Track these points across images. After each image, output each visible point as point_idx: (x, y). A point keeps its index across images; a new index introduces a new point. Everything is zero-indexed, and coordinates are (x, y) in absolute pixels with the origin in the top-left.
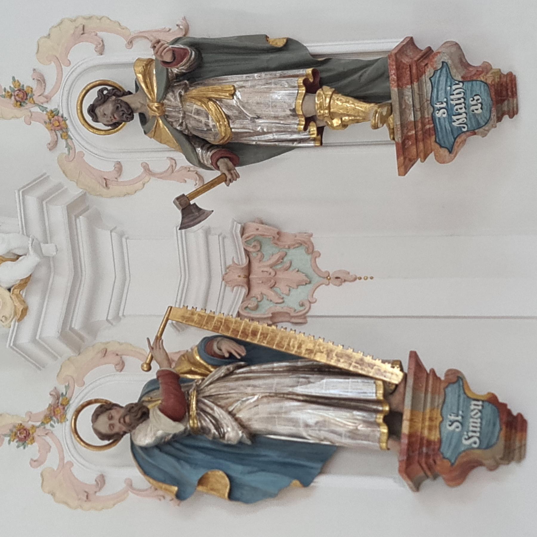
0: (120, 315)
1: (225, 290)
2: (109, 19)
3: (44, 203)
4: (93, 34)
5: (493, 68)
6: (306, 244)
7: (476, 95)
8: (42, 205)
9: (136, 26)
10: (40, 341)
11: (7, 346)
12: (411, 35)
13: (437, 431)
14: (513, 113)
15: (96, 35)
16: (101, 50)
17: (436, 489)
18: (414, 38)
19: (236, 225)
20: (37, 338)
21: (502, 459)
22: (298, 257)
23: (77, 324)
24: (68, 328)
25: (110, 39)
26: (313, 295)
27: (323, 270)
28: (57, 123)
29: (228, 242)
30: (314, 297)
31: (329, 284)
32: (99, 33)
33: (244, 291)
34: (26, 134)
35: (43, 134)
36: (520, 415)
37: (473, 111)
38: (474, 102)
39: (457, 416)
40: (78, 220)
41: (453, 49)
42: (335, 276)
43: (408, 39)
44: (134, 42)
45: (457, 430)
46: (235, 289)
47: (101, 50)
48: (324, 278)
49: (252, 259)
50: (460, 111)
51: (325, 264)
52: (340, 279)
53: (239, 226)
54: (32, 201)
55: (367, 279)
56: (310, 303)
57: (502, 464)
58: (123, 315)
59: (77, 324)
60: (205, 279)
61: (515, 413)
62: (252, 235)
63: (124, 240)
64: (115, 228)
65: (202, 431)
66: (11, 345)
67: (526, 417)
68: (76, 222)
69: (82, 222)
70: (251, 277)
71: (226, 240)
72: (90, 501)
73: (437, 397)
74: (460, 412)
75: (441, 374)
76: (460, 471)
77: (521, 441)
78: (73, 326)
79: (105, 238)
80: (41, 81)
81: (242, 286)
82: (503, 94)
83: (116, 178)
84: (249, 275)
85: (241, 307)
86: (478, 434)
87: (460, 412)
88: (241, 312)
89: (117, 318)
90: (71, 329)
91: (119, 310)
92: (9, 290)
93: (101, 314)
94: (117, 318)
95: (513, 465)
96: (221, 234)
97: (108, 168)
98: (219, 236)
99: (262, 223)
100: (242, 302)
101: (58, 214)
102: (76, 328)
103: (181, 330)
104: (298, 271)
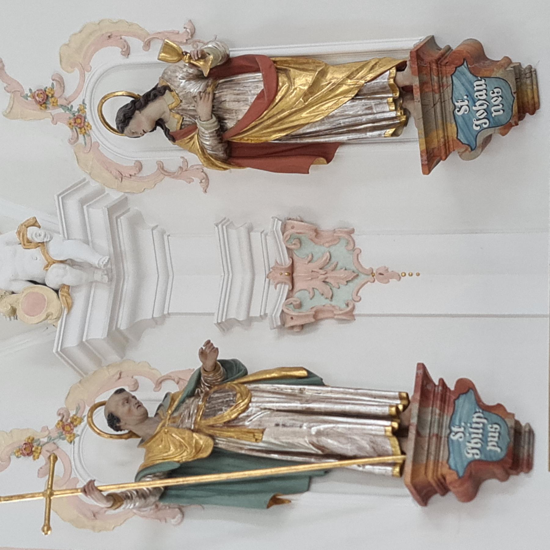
0: (166, 312)
1: (269, 287)
3: (85, 207)
4: (119, 38)
5: (513, 61)
7: (495, 88)
8: (83, 209)
9: (152, 27)
10: (86, 343)
11: (54, 351)
13: (446, 440)
15: (121, 38)
16: (127, 52)
20: (84, 340)
23: (123, 324)
24: (114, 328)
25: (136, 44)
26: (358, 292)
27: (367, 268)
28: (79, 123)
29: (270, 240)
30: (359, 295)
31: (374, 281)
32: (123, 37)
33: (287, 288)
34: (49, 135)
35: (64, 130)
37: (477, 96)
38: (493, 430)
39: (460, 427)
40: (119, 220)
41: (508, 60)
42: (379, 272)
44: (152, 43)
45: (466, 113)
46: (278, 286)
47: (127, 52)
48: (368, 275)
49: (295, 257)
51: (368, 261)
52: (383, 275)
53: (280, 223)
54: (72, 204)
55: (412, 275)
59: (123, 324)
60: (248, 277)
64: (157, 226)
66: (59, 350)
68: (117, 223)
69: (123, 222)
70: (294, 275)
72: (96, 519)
74: (463, 424)
78: (118, 326)
79: (146, 237)
80: (61, 82)
81: (285, 283)
83: (130, 175)
84: (293, 273)
85: (286, 305)
87: (463, 424)
88: (285, 310)
89: (164, 317)
90: (117, 329)
92: (57, 291)
96: (263, 231)
98: (261, 233)
100: (286, 299)
101: (98, 216)
103: (226, 330)
104: (346, 269)
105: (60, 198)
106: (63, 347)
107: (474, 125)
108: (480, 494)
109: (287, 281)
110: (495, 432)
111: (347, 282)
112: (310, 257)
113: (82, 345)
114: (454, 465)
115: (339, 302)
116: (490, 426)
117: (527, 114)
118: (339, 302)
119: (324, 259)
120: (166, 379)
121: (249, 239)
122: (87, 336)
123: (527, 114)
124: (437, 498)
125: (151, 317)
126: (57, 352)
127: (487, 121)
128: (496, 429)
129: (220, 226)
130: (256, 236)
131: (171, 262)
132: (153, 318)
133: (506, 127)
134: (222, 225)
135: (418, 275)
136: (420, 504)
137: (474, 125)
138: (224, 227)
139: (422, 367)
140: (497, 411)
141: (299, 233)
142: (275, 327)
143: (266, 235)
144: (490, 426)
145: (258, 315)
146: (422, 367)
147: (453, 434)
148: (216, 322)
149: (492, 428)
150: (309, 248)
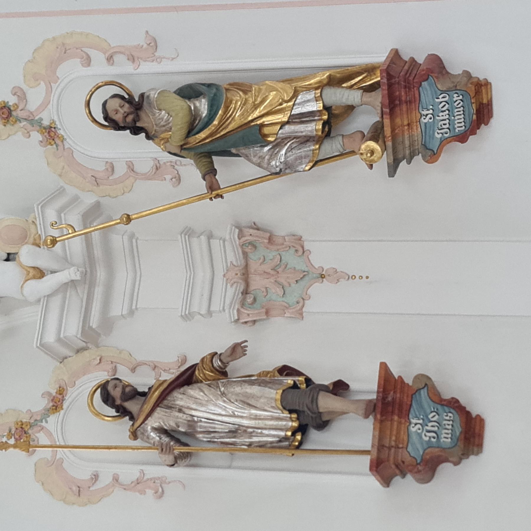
0: (134, 307)
2: (106, 41)
3: (62, 215)
6: (298, 244)
11: (35, 346)
12: (395, 47)
14: (480, 446)
17: (407, 485)
18: (399, 50)
19: (234, 230)
20: (62, 336)
21: (463, 454)
22: (292, 260)
23: (94, 322)
24: (87, 326)
36: (478, 416)
38: (448, 418)
43: (394, 52)
45: (430, 121)
46: (235, 285)
50: (444, 127)
56: (303, 299)
57: (464, 459)
58: (136, 309)
59: (94, 322)
61: (474, 415)
62: (249, 240)
63: (134, 241)
65: (203, 106)
66: (38, 345)
67: (484, 416)
71: (226, 242)
73: (413, 104)
75: (409, 380)
76: (427, 467)
77: (487, 93)
78: (91, 325)
82: (471, 434)
86: (447, 126)
89: (131, 312)
90: (90, 328)
91: (132, 304)
93: (118, 308)
94: (131, 312)
95: (472, 458)
97: (100, 167)
99: (258, 229)
102: (94, 327)
105: (40, 207)
106: (43, 342)
107: (436, 133)
108: (436, 475)
109: (240, 281)
110: (449, 420)
111: (296, 281)
112: (262, 258)
113: (59, 340)
114: (415, 450)
115: (291, 299)
116: (446, 414)
117: (483, 125)
118: (291, 299)
119: (276, 260)
120: (137, 366)
121: (210, 246)
122: (64, 332)
123: (483, 125)
124: (398, 479)
125: (120, 314)
126: (37, 347)
127: (448, 130)
128: (450, 417)
129: (183, 235)
130: (216, 244)
131: (139, 285)
132: (122, 315)
133: (462, 138)
134: (186, 235)
135: (367, 277)
136: (384, 487)
137: (436, 133)
138: (187, 236)
139: (384, 367)
140: (454, 404)
141: (254, 238)
142: (233, 320)
143: (224, 241)
144: (446, 414)
145: (218, 310)
146: (384, 367)
147: (413, 425)
148: (180, 315)
149: (447, 416)
150: (262, 251)
